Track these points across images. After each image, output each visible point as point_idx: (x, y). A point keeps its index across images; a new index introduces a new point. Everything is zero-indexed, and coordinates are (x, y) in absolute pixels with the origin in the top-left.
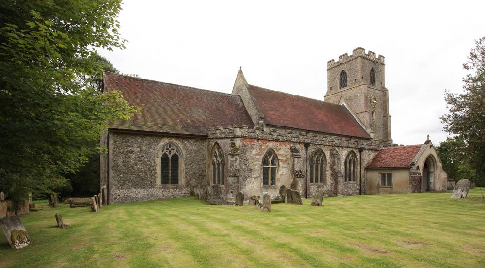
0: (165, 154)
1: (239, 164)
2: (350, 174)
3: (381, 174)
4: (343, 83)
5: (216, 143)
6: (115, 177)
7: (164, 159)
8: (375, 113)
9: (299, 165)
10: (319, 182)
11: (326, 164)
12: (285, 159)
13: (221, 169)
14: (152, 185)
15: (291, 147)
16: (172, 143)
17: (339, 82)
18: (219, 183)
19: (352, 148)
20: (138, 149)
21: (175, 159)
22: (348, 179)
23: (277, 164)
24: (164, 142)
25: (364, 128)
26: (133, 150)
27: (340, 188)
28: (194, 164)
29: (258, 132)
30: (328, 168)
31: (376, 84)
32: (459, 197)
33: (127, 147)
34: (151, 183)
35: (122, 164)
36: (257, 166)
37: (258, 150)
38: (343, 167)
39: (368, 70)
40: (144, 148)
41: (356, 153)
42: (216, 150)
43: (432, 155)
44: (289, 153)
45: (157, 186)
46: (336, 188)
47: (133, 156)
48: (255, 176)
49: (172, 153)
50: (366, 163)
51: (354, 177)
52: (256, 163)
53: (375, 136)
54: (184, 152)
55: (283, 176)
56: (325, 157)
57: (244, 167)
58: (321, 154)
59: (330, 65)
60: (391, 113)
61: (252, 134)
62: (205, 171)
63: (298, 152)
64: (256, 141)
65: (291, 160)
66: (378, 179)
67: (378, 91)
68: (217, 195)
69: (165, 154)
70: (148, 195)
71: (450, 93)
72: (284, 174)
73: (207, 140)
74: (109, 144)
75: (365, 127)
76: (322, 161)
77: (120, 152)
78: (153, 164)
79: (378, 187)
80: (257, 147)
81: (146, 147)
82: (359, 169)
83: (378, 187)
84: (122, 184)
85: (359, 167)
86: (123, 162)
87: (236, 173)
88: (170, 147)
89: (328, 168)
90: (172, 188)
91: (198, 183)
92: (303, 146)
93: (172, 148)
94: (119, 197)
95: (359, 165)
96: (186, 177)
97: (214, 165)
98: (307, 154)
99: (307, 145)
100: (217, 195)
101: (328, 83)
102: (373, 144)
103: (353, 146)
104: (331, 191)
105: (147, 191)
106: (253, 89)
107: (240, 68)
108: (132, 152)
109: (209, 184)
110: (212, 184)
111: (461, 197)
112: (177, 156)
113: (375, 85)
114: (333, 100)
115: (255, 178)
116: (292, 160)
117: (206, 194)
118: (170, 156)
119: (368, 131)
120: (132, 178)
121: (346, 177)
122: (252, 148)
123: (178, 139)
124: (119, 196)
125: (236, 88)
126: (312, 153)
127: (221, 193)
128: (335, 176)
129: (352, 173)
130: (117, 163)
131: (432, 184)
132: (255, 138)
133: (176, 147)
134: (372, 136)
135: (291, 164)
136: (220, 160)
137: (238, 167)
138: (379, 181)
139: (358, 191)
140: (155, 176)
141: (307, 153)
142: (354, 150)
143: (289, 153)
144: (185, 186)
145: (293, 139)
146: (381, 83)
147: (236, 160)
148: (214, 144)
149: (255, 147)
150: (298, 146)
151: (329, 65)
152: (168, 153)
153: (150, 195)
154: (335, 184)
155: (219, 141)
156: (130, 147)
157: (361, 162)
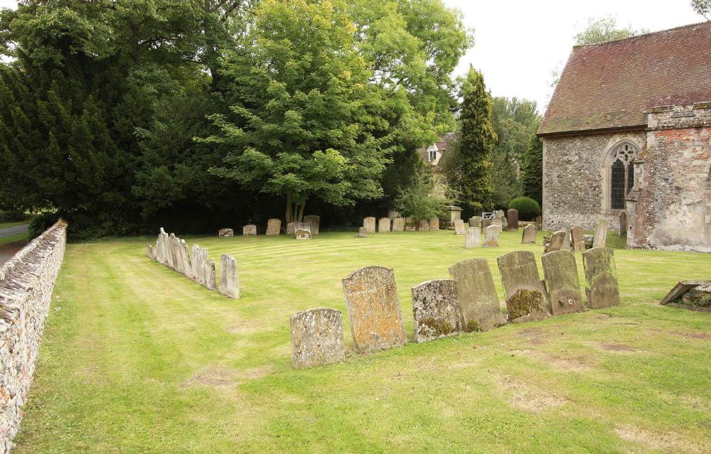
0: (618, 160)
6: (549, 196)
14: (596, 209)
16: (628, 143)
24: (616, 140)
33: (562, 155)
34: (594, 206)
40: (584, 155)
45: (602, 212)
47: (570, 167)
48: (690, 201)
49: (630, 159)
52: (693, 175)
57: (662, 184)
64: (693, 131)
70: (589, 224)
71: (477, 68)
80: (697, 143)
84: (557, 206)
86: (558, 177)
93: (629, 149)
94: (552, 224)
105: (588, 217)
108: (569, 162)
115: (688, 205)
122: (683, 146)
123: (637, 133)
130: (552, 179)
132: (690, 127)
140: (600, 195)
149: (688, 144)
156: (566, 155)
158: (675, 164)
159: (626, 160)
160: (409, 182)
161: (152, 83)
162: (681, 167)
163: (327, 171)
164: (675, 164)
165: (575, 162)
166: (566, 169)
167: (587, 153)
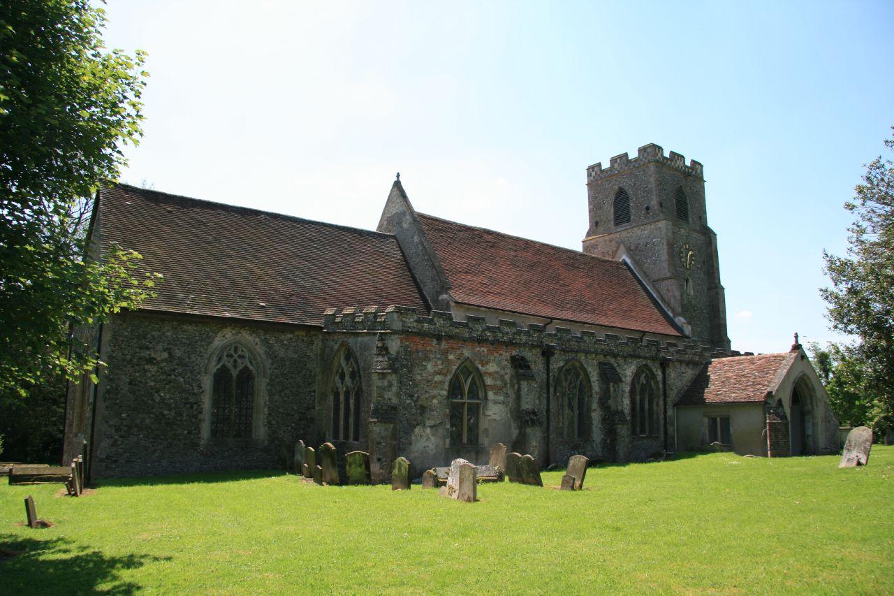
0: (224, 366)
1: (398, 395)
7: (222, 378)
8: (690, 281)
11: (591, 396)
12: (499, 383)
13: (352, 406)
17: (612, 211)
18: (346, 437)
19: (645, 358)
21: (246, 377)
22: (638, 429)
23: (481, 394)
25: (671, 315)
26: (153, 355)
28: (287, 392)
29: (440, 322)
30: (595, 406)
31: (690, 220)
32: (854, 464)
33: (140, 348)
34: (189, 433)
36: (437, 397)
37: (439, 362)
38: (627, 402)
41: (654, 370)
43: (807, 375)
44: (508, 371)
48: (432, 422)
50: (675, 391)
52: (435, 392)
54: (268, 363)
56: (589, 381)
57: (408, 402)
59: (593, 174)
60: (724, 281)
61: (426, 325)
62: (314, 408)
63: (528, 367)
65: (512, 386)
67: (695, 235)
69: (224, 366)
74: (103, 343)
75: (673, 311)
76: (581, 390)
77: (124, 360)
80: (438, 356)
81: (182, 349)
82: (662, 407)
85: (661, 403)
86: (130, 383)
88: (236, 351)
89: (595, 406)
93: (240, 353)
95: (661, 398)
96: (269, 422)
98: (548, 374)
99: (547, 353)
101: (590, 212)
102: (689, 351)
107: (398, 175)
108: (151, 361)
111: (859, 464)
112: (251, 371)
113: (687, 220)
115: (431, 427)
116: (516, 386)
118: (235, 373)
120: (147, 421)
122: (427, 359)
125: (390, 218)
126: (560, 369)
128: (611, 418)
129: (647, 415)
131: (811, 439)
135: (512, 396)
137: (395, 401)
140: (200, 416)
143: (509, 372)
146: (700, 218)
147: (390, 385)
149: (432, 356)
152: (230, 365)
156: (148, 348)
158: (419, 377)
159: (235, 367)
160: (820, 357)
163: (76, 58)
165: (163, 361)
167: (182, 349)
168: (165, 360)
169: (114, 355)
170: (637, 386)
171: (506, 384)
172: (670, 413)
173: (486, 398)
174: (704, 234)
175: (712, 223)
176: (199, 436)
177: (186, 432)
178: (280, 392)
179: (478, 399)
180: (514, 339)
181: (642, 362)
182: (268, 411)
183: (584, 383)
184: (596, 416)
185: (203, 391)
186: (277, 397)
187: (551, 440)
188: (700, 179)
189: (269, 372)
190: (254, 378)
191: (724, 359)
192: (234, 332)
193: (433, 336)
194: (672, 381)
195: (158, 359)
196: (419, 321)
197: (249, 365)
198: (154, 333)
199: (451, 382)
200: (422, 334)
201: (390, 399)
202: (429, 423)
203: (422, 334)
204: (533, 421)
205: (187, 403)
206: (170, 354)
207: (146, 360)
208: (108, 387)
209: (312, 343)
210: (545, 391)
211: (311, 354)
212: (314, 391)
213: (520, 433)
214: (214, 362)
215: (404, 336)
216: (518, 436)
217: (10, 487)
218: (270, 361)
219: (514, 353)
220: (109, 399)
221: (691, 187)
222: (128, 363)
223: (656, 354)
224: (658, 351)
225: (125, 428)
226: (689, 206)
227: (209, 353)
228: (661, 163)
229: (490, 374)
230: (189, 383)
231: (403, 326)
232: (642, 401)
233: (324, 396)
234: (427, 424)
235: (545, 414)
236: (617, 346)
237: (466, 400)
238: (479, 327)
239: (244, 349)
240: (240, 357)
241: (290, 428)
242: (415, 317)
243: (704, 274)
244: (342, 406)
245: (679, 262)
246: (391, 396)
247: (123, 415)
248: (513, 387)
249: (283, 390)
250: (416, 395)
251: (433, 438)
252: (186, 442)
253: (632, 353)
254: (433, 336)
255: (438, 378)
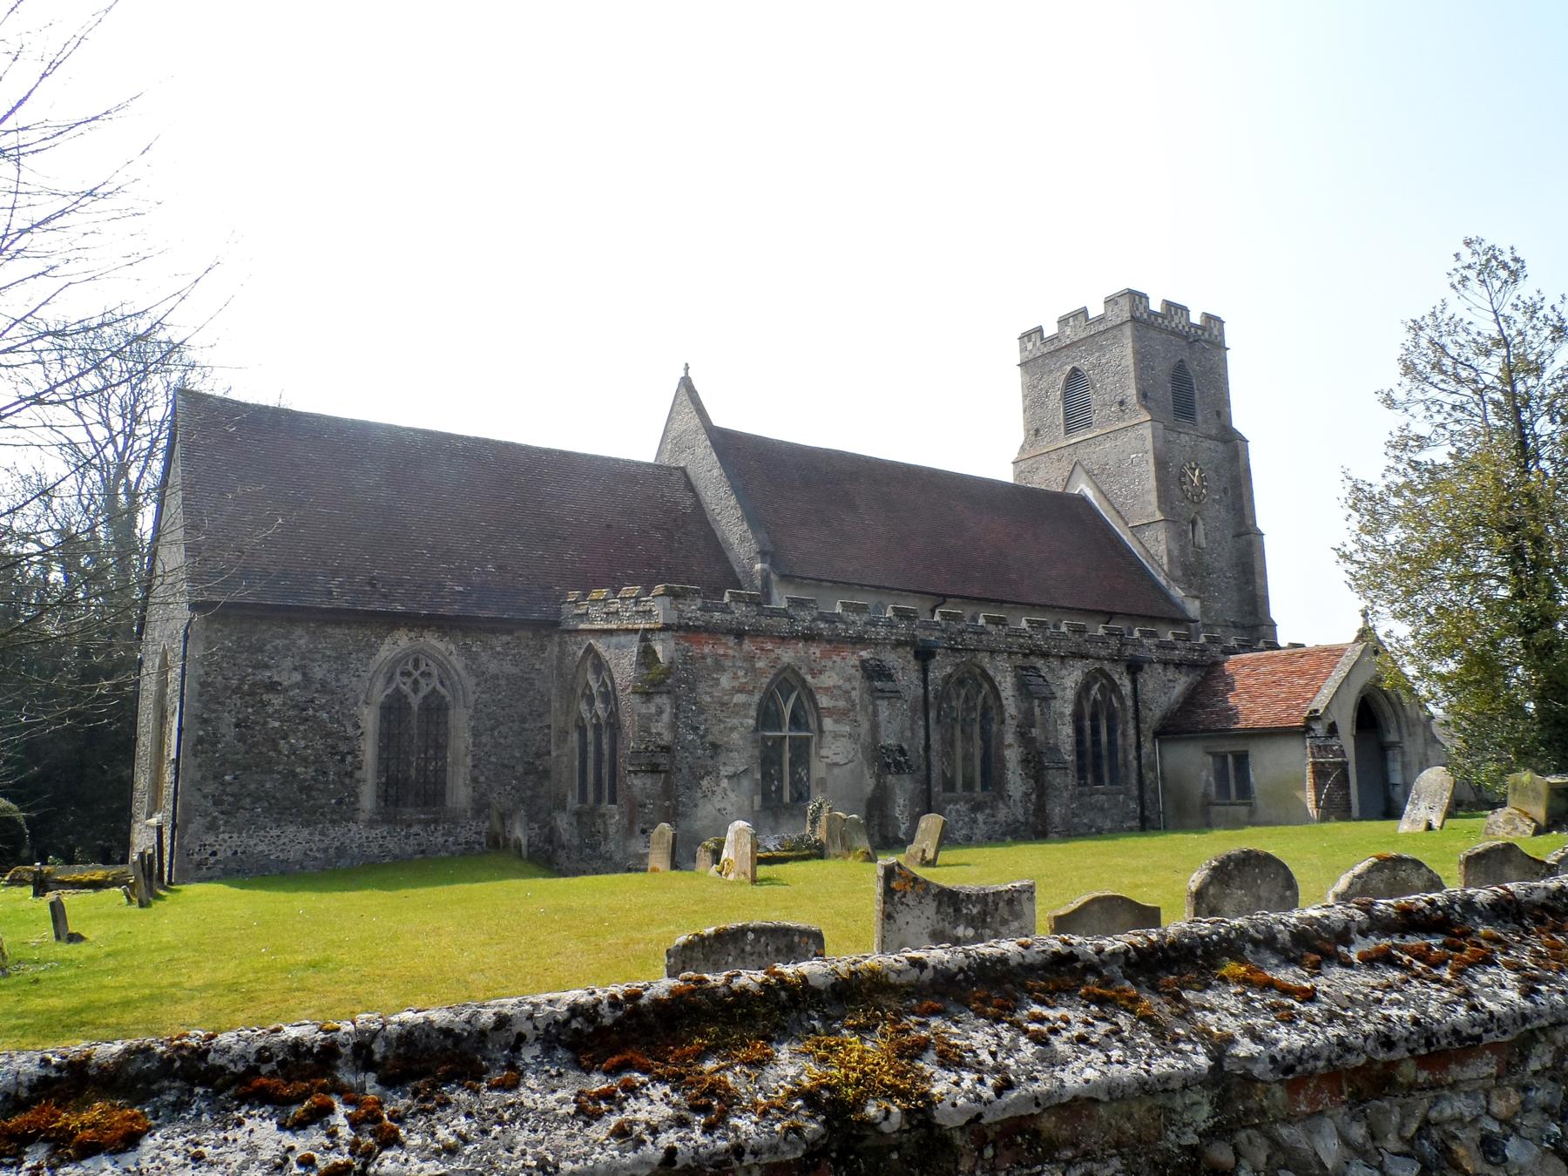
0: (397, 690)
1: (673, 727)
2: (1097, 756)
3: (1214, 755)
4: (1075, 417)
5: (590, 649)
7: (393, 710)
8: (1200, 522)
9: (894, 726)
10: (978, 789)
11: (1003, 722)
12: (842, 704)
13: (605, 747)
14: (345, 810)
15: (863, 662)
18: (599, 800)
19: (1098, 658)
20: (297, 677)
21: (436, 709)
23: (813, 724)
24: (401, 642)
26: (276, 679)
27: (1056, 811)
30: (1009, 738)
31: (1199, 418)
32: (1423, 826)
33: (254, 667)
34: (340, 802)
35: (233, 731)
36: (738, 732)
37: (741, 673)
38: (1066, 731)
39: (1163, 369)
40: (318, 672)
41: (1116, 677)
42: (591, 677)
44: (856, 684)
46: (1040, 809)
47: (277, 701)
48: (730, 770)
51: (1114, 768)
52: (735, 721)
53: (1205, 611)
54: (471, 683)
55: (836, 771)
56: (998, 697)
57: (690, 737)
58: (980, 686)
59: (1030, 346)
60: (1262, 523)
62: (549, 753)
63: (890, 677)
64: (731, 641)
66: (1204, 774)
67: (1207, 444)
68: (591, 847)
69: (397, 690)
70: (325, 850)
72: (840, 759)
73: (556, 639)
76: (985, 715)
78: (350, 730)
79: (1207, 804)
83: (1207, 804)
85: (1131, 732)
86: (237, 725)
87: (662, 760)
88: (416, 666)
89: (1009, 738)
90: (419, 822)
91: (522, 801)
92: (910, 657)
93: (423, 668)
94: (212, 860)
96: (475, 780)
97: (582, 730)
99: (924, 654)
100: (594, 847)
102: (1180, 644)
103: (1103, 653)
104: (1026, 823)
105: (322, 833)
106: (730, 446)
107: (687, 368)
109: (561, 805)
110: (572, 802)
111: (1429, 827)
112: (443, 697)
114: (1047, 479)
115: (729, 777)
117: (551, 842)
118: (415, 701)
119: (1178, 593)
121: (1081, 771)
122: (719, 667)
124: (214, 854)
127: (606, 837)
128: (1037, 762)
130: (216, 730)
133: (440, 665)
134: (1193, 608)
135: (865, 726)
136: (602, 714)
137: (667, 737)
138: (1208, 783)
139: (1136, 823)
140: (358, 774)
141: (925, 681)
142: (1107, 666)
144: (469, 814)
145: (872, 632)
146: (1218, 414)
147: (660, 712)
148: (581, 653)
149: (728, 663)
150: (891, 658)
151: (1023, 349)
152: (406, 689)
153: (332, 851)
154: (1038, 796)
155: (599, 645)
156: (267, 667)
157: (1137, 711)
159: (415, 691)
161: (1219, 1138)
162: (717, 707)
164: (708, 699)
165: (292, 687)
166: (264, 705)
168: (297, 685)
169: (210, 680)
170: (1085, 703)
171: (854, 706)
172: (1147, 747)
173: (821, 731)
174: (1225, 442)
175: (1241, 421)
176: (357, 806)
177: (333, 801)
178: (492, 729)
179: (808, 729)
180: (866, 632)
181: (1092, 665)
182: (473, 760)
183: (990, 702)
184: (1012, 755)
185: (362, 734)
186: (484, 739)
187: (933, 795)
188: (1219, 346)
189: (472, 698)
190: (447, 709)
191: (1244, 656)
192: (412, 635)
193: (729, 632)
194: (1150, 695)
195: (286, 683)
196: (703, 609)
197: (439, 687)
198: (278, 641)
199: (760, 705)
200: (712, 631)
201: (659, 734)
202: (725, 771)
203: (712, 631)
204: (898, 764)
205: (335, 754)
206: (304, 675)
207: (265, 686)
208: (201, 733)
209: (543, 648)
210: (919, 714)
211: (542, 667)
212: (549, 727)
213: (878, 785)
214: (380, 683)
215: (682, 633)
216: (874, 790)
217: (38, 900)
218: (474, 680)
219: (865, 654)
220: (202, 752)
221: (1200, 361)
222: (234, 692)
223: (1119, 650)
224: (1122, 645)
225: (231, 799)
226: (1197, 395)
227: (372, 670)
228: (1145, 322)
229: (827, 689)
230: (338, 722)
231: (680, 617)
232: (1096, 731)
233: (564, 734)
234: (723, 773)
235: (921, 752)
236: (1046, 639)
237: (786, 732)
238: (805, 616)
239: (430, 662)
240: (409, 674)
241: (508, 788)
242: (699, 602)
243: (1228, 511)
244: (591, 749)
245: (1177, 491)
246: (661, 729)
247: (227, 778)
248: (866, 711)
249: (497, 727)
250: (702, 727)
251: (732, 795)
252: (334, 817)
253: (1074, 650)
254: (729, 632)
255: (739, 698)
